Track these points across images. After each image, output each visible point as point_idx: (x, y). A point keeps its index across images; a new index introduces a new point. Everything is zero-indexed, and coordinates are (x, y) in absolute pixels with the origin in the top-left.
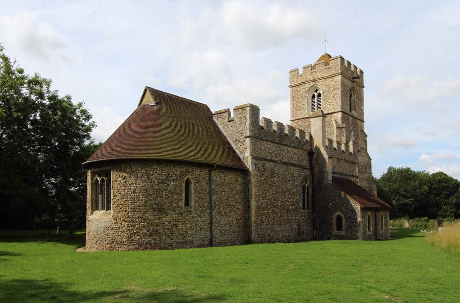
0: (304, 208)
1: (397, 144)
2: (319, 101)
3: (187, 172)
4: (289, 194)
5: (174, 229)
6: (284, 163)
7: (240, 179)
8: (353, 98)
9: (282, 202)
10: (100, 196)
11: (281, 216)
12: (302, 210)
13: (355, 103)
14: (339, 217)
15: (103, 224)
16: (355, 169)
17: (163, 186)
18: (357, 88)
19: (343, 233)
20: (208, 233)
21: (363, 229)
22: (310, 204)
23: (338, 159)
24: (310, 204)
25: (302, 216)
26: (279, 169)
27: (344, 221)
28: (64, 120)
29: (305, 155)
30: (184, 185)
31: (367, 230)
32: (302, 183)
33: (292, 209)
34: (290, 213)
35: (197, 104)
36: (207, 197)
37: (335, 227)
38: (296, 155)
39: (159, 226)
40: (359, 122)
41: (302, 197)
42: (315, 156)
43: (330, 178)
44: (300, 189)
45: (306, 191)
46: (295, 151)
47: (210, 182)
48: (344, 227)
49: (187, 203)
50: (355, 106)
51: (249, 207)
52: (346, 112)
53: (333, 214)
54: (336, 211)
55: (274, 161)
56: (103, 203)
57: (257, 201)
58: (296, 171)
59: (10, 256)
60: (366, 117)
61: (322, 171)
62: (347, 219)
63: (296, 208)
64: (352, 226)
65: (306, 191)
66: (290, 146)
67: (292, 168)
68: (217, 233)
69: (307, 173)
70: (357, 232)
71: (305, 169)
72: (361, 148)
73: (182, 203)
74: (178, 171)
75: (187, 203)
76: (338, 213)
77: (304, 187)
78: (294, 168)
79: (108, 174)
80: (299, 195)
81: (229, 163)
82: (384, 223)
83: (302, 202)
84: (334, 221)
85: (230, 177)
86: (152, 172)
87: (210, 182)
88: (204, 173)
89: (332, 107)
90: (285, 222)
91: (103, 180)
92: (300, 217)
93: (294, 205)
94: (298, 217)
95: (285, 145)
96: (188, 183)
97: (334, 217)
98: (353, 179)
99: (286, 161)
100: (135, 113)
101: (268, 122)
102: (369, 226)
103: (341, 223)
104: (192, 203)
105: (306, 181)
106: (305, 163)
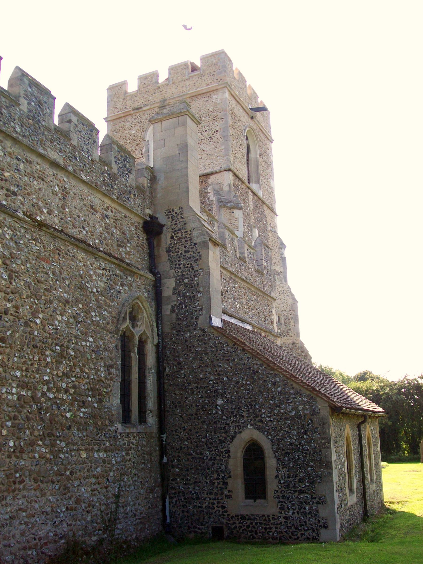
0: (126, 418)
4: (62, 356)
8: (252, 155)
9: (23, 385)
11: (19, 451)
12: (119, 426)
13: (257, 166)
14: (254, 452)
19: (269, 507)
22: (151, 403)
25: (119, 449)
27: (271, 462)
28: (391, 461)
29: (131, 225)
31: (347, 491)
32: (118, 319)
33: (74, 421)
34: (65, 438)
37: (237, 485)
38: (98, 215)
40: (267, 212)
41: (117, 373)
42: (166, 238)
44: (112, 342)
45: (134, 355)
46: (97, 199)
48: (272, 485)
50: (258, 174)
52: (240, 176)
53: (233, 437)
54: (240, 428)
61: (189, 286)
63: (94, 417)
64: (301, 480)
65: (134, 355)
67: (80, 255)
70: (322, 501)
71: (133, 274)
76: (250, 433)
78: (90, 260)
80: (108, 367)
83: (118, 392)
84: (236, 463)
89: (208, 162)
90: (39, 478)
93: (84, 404)
94: (102, 455)
97: (237, 449)
102: (350, 478)
103: (261, 471)
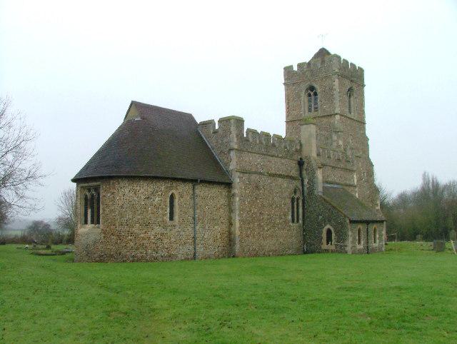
0: (293, 221)
1: (403, 156)
2: (316, 99)
3: (171, 188)
5: (159, 242)
6: (270, 175)
7: (225, 192)
10: (89, 211)
15: (92, 238)
16: (353, 178)
17: (148, 202)
18: (355, 87)
20: (191, 248)
21: (353, 242)
22: (301, 217)
23: (333, 167)
24: (301, 217)
26: (265, 181)
27: (333, 235)
29: (294, 165)
30: (168, 200)
35: (185, 116)
36: (191, 210)
37: (324, 240)
39: (145, 239)
42: (306, 165)
43: (320, 189)
44: (289, 201)
47: (194, 196)
49: (171, 218)
51: (116, 176)
54: (325, 225)
55: (261, 173)
56: (92, 216)
57: (240, 215)
58: (285, 183)
59: (175, 213)
60: (368, 119)
62: (337, 232)
66: (278, 156)
68: (200, 249)
69: (298, 183)
70: (346, 246)
72: (355, 153)
73: (167, 218)
74: (162, 186)
75: (171, 218)
76: (328, 226)
77: (293, 200)
79: (97, 189)
81: (218, 178)
82: (378, 236)
85: (215, 191)
86: (138, 188)
87: (194, 196)
88: (188, 187)
91: (92, 196)
92: (291, 233)
95: (272, 156)
96: (172, 198)
98: (350, 190)
99: (273, 172)
100: (121, 130)
101: (254, 132)
104: (176, 217)
105: (295, 192)
106: (294, 173)
